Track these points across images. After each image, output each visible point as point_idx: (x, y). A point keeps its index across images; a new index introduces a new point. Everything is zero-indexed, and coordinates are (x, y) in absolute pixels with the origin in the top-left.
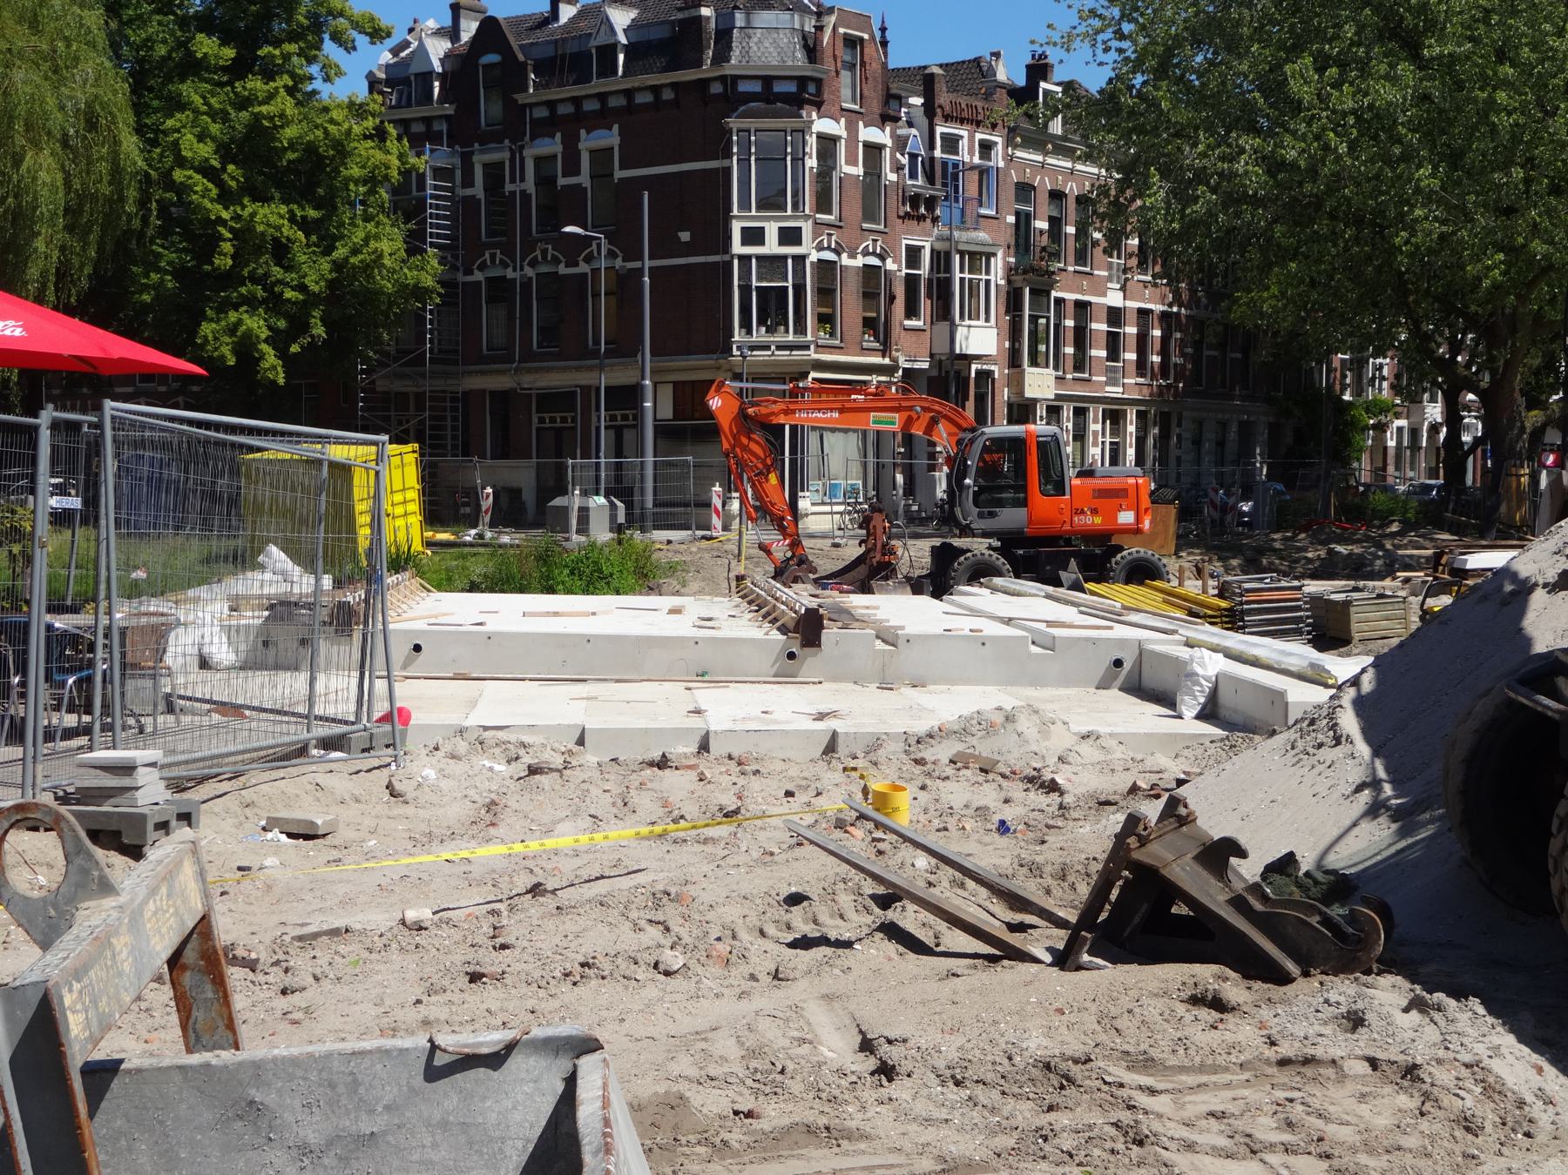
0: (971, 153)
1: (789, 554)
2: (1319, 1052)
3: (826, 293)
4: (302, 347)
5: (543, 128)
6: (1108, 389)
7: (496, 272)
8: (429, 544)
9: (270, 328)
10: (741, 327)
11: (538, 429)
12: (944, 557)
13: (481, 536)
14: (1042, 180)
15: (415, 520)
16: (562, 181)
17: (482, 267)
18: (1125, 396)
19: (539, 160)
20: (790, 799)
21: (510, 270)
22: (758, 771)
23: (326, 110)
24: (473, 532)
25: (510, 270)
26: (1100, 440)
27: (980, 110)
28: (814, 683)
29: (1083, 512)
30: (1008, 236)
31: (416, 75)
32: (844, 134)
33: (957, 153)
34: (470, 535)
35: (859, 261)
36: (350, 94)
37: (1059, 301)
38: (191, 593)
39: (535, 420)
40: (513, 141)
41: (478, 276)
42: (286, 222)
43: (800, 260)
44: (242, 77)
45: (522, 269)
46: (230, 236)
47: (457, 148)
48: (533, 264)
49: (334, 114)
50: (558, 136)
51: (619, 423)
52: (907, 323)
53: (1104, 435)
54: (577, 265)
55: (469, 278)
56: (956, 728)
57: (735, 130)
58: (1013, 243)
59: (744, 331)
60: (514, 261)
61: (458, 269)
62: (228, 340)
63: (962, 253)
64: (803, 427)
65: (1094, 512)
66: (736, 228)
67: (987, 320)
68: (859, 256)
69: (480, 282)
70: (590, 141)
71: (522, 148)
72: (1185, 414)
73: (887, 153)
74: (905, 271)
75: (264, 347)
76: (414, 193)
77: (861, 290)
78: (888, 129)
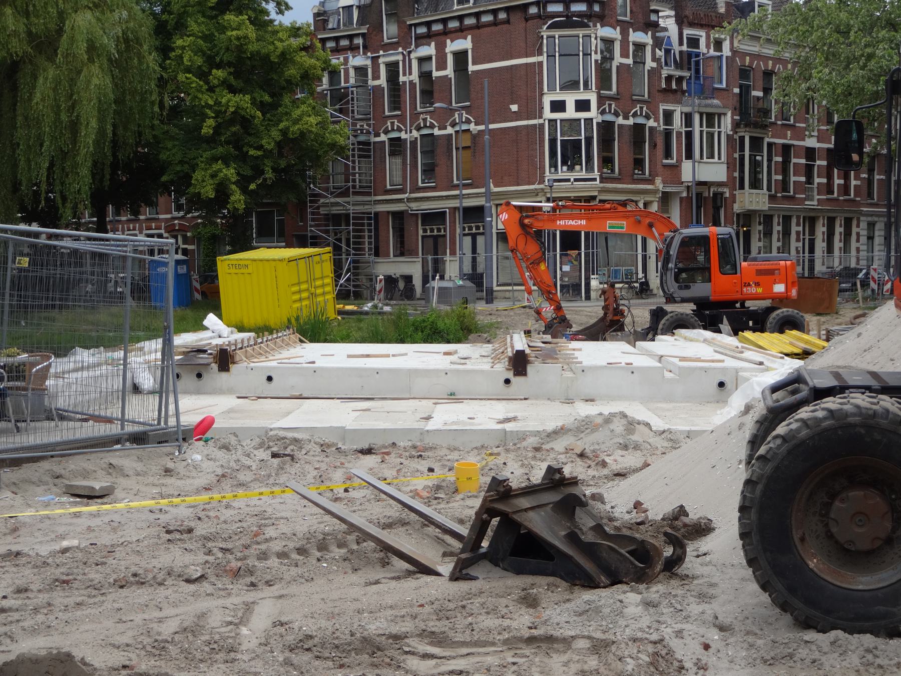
0: (708, 46)
1: (554, 315)
2: (557, 633)
3: (606, 141)
4: (257, 185)
5: (422, 40)
6: (807, 203)
7: (394, 135)
8: (340, 313)
9: (238, 174)
10: (550, 167)
11: (423, 237)
12: (657, 314)
13: (375, 307)
14: (758, 64)
15: (330, 297)
16: (435, 74)
17: (386, 132)
18: (819, 207)
19: (422, 60)
20: (431, 474)
21: (403, 132)
22: (421, 456)
23: (275, 32)
24: (370, 305)
25: (403, 132)
26: (802, 237)
27: (714, 18)
28: (521, 399)
29: (749, 285)
30: (735, 101)
31: (343, 8)
32: (619, 37)
33: (698, 48)
34: (367, 307)
35: (631, 121)
36: (291, 21)
37: (770, 145)
38: (139, 345)
39: (421, 232)
40: (404, 49)
41: (383, 138)
42: (249, 105)
43: (589, 121)
44: (223, 12)
45: (411, 132)
46: (213, 115)
47: (369, 54)
48: (419, 129)
49: (280, 35)
50: (433, 44)
51: (474, 231)
52: (665, 161)
53: (804, 234)
54: (445, 128)
55: (377, 139)
56: (572, 427)
57: (545, 37)
58: (738, 106)
59: (553, 170)
60: (406, 127)
61: (370, 133)
62: (211, 182)
63: (701, 114)
64: (593, 233)
65: (757, 284)
66: (547, 101)
67: (719, 158)
68: (631, 118)
69: (385, 142)
70: (453, 46)
71: (410, 52)
72: (862, 218)
73: (649, 49)
74: (662, 127)
75: (234, 187)
76: (343, 84)
77: (632, 140)
78: (650, 33)
